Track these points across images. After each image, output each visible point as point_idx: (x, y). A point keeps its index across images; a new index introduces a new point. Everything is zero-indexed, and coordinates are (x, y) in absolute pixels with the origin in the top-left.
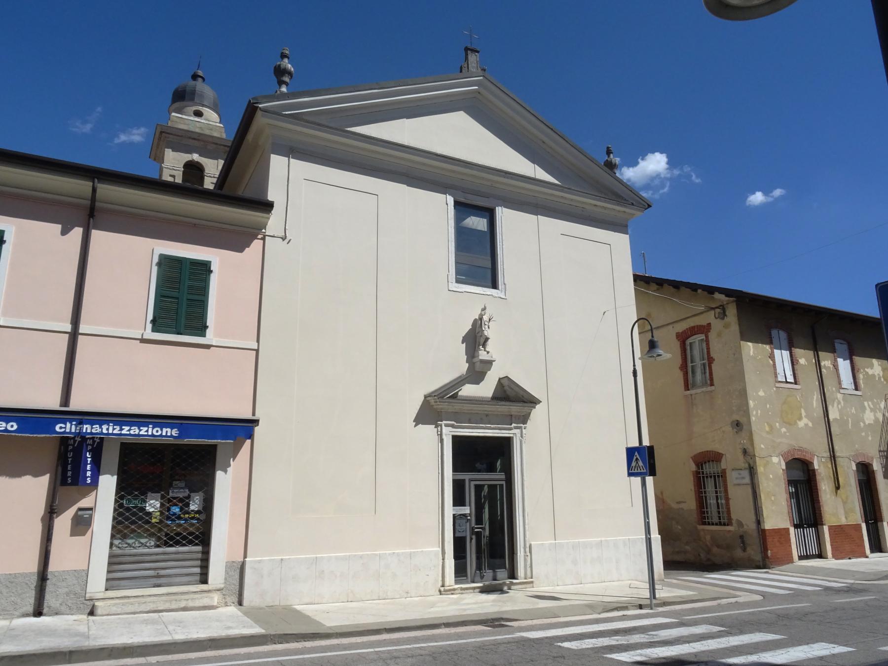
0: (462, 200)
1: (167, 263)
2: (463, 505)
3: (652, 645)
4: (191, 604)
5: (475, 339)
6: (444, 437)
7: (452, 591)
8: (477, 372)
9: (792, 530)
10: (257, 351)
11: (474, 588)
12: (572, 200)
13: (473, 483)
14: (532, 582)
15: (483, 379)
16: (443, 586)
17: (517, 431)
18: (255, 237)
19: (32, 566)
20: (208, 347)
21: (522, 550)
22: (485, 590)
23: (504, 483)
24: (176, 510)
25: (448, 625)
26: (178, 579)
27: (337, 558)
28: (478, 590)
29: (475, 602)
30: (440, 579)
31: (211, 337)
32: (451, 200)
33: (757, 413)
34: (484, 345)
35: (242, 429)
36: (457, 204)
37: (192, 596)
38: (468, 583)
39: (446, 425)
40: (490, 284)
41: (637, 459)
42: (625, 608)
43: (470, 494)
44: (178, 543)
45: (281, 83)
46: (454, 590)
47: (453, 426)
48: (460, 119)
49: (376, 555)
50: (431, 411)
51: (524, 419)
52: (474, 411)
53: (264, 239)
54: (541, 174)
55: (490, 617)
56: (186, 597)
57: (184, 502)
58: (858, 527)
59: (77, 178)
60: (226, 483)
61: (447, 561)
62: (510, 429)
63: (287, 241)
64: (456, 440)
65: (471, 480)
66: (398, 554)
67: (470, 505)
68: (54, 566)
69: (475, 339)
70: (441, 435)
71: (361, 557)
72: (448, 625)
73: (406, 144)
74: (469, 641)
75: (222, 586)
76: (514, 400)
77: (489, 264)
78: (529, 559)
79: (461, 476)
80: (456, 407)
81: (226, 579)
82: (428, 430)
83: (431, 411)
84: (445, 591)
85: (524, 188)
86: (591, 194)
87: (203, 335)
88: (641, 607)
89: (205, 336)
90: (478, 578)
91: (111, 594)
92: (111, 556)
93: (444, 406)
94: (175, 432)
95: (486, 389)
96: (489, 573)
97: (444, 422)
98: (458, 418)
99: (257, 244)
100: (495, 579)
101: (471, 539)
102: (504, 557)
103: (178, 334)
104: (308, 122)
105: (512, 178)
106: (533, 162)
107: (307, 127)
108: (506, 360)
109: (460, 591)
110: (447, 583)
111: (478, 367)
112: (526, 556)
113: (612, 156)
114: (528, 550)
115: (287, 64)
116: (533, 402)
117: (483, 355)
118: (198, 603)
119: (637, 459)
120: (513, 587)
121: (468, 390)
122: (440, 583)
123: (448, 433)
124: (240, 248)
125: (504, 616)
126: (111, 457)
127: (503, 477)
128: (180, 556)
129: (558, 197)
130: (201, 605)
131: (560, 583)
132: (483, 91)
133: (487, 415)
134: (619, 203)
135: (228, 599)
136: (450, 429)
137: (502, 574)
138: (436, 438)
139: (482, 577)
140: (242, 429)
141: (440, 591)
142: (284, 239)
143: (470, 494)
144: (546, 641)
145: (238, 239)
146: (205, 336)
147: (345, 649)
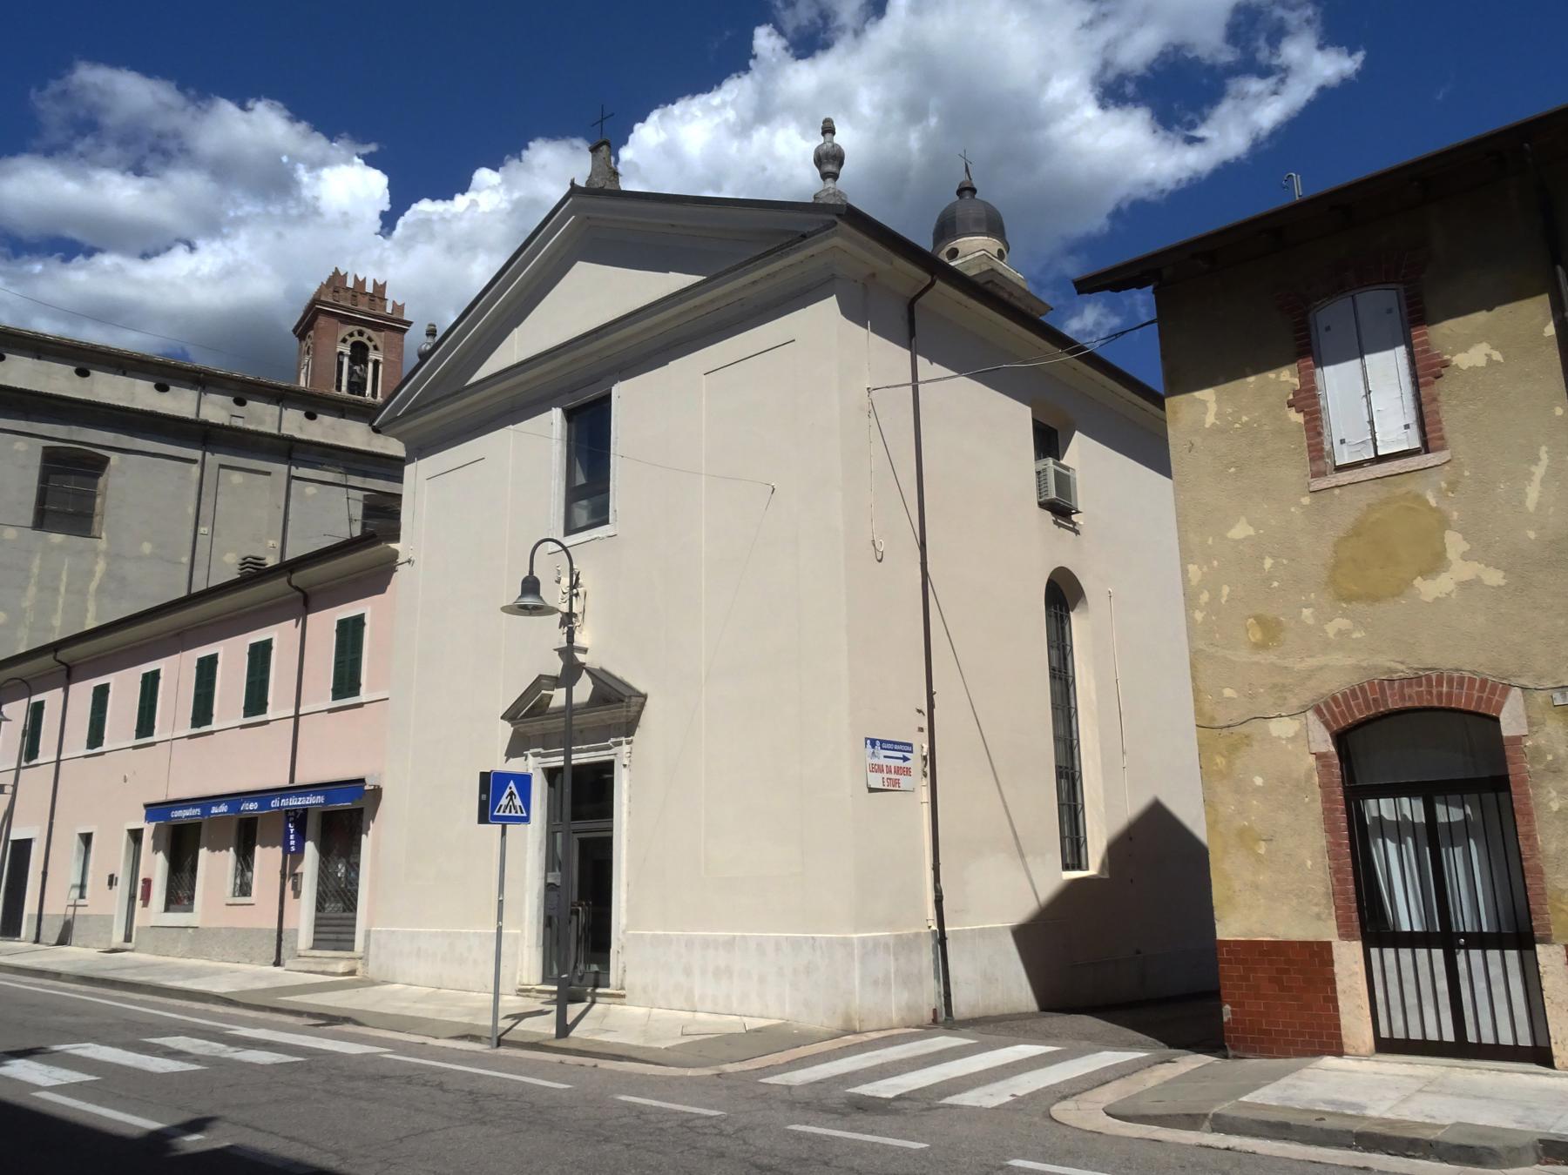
7: (994, 1026)
9: (1348, 957)
12: (712, 301)
13: (577, 836)
14: (623, 996)
19: (276, 926)
31: (364, 696)
33: (1215, 597)
36: (569, 415)
39: (535, 755)
41: (511, 794)
42: (619, 1058)
47: (543, 756)
48: (583, 273)
51: (628, 728)
54: (677, 281)
58: (1320, 954)
62: (609, 748)
68: (45, 912)
73: (515, 362)
87: (357, 694)
91: (317, 953)
92: (317, 918)
94: (320, 799)
105: (607, 334)
119: (511, 794)
125: (634, 1054)
126: (312, 825)
129: (690, 310)
136: (539, 759)
147: (168, 1010)
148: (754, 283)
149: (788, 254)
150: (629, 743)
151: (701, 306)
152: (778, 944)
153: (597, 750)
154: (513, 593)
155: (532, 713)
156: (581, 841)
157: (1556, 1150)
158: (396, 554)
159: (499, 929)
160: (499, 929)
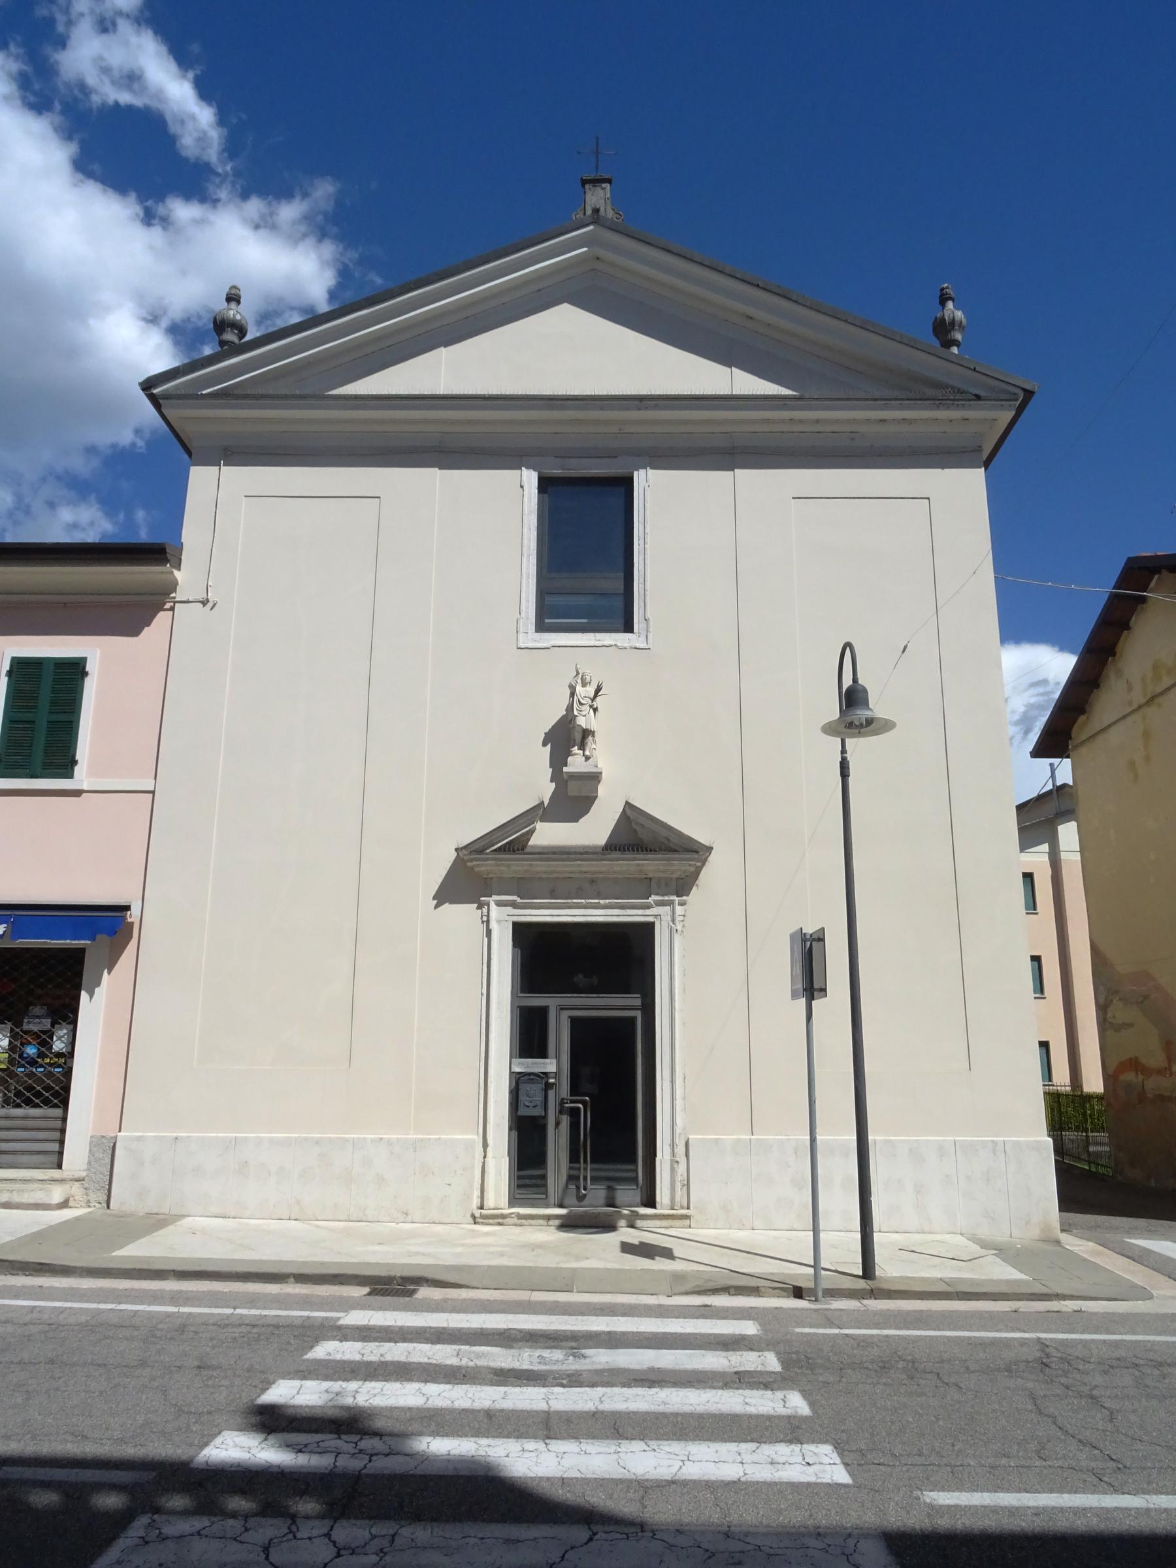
0: (557, 472)
1: (22, 670)
2: (543, 1054)
3: (574, 1380)
4: (16, 1198)
5: (566, 737)
6: (494, 925)
7: (499, 1219)
8: (572, 797)
10: (153, 792)
11: (549, 1218)
12: (817, 421)
14: (687, 1217)
15: (587, 811)
16: (482, 1208)
17: (664, 911)
18: (160, 607)
20: (77, 793)
21: (667, 1150)
22: (568, 1224)
23: (638, 1014)
24: (31, 1051)
25: (302, 1278)
26: (25, 1159)
27: (271, 1140)
28: (557, 1222)
29: (536, 1240)
30: (477, 1193)
31: (82, 777)
32: (530, 478)
34: (582, 746)
35: (109, 924)
36: (545, 484)
37: (17, 1186)
38: (547, 1206)
39: (499, 904)
40: (622, 627)
42: (754, 1291)
43: (560, 1035)
44: (29, 1103)
45: (948, 343)
46: (504, 1216)
47: (514, 905)
48: (566, 320)
49: (346, 1140)
50: (471, 877)
51: (683, 886)
52: (569, 873)
53: (172, 609)
55: (398, 1273)
56: (9, 1186)
57: (44, 1040)
59: (18, 566)
60: (95, 1010)
61: (490, 1162)
62: (648, 907)
63: (210, 605)
64: (521, 932)
65: (562, 1008)
66: (390, 1143)
67: (558, 1057)
69: (566, 737)
70: (488, 921)
71: (317, 1142)
72: (302, 1278)
74: (265, 1312)
75: (84, 1174)
76: (654, 851)
77: (620, 586)
78: (681, 1169)
79: (537, 1000)
80: (515, 866)
81: (89, 1163)
82: (464, 914)
83: (471, 877)
84: (482, 1217)
85: (426, 421)
86: (852, 398)
87: (69, 775)
88: (798, 1293)
89: (72, 777)
90: (571, 1199)
93: (486, 866)
95: (594, 829)
96: (597, 1193)
97: (495, 897)
98: (525, 888)
99: (162, 618)
100: (611, 1203)
101: (557, 1124)
102: (634, 1161)
103: (32, 777)
104: (246, 396)
105: (656, 407)
106: (729, 365)
107: (832, 409)
108: (628, 774)
109: (515, 1220)
110: (490, 1202)
111: (573, 789)
112: (674, 1162)
113: (950, 305)
114: (680, 1150)
115: (952, 310)
116: (696, 852)
117: (576, 763)
118: (26, 1198)
120: (639, 1223)
121: (547, 834)
122: (476, 1202)
123: (503, 917)
124: (133, 629)
125: (430, 1276)
127: (638, 1002)
128: (30, 1123)
129: (783, 421)
130: (31, 1201)
131: (757, 1224)
132: (602, 253)
133: (593, 881)
134: (939, 402)
135: (92, 1197)
136: (510, 910)
137: (627, 1194)
138: (480, 929)
139: (581, 1198)
140: (109, 924)
141: (473, 1216)
142: (204, 603)
143: (560, 1035)
144: (603, 1336)
145: (130, 614)
146: (72, 777)
148: (883, 421)
149: (938, 407)
150: (682, 904)
151: (801, 421)
152: (941, 1150)
153: (622, 907)
154: (832, 710)
155: (509, 848)
156: (574, 1021)
157: (1173, 1297)
158: (173, 586)
159: (813, 1140)
160: (813, 1140)
